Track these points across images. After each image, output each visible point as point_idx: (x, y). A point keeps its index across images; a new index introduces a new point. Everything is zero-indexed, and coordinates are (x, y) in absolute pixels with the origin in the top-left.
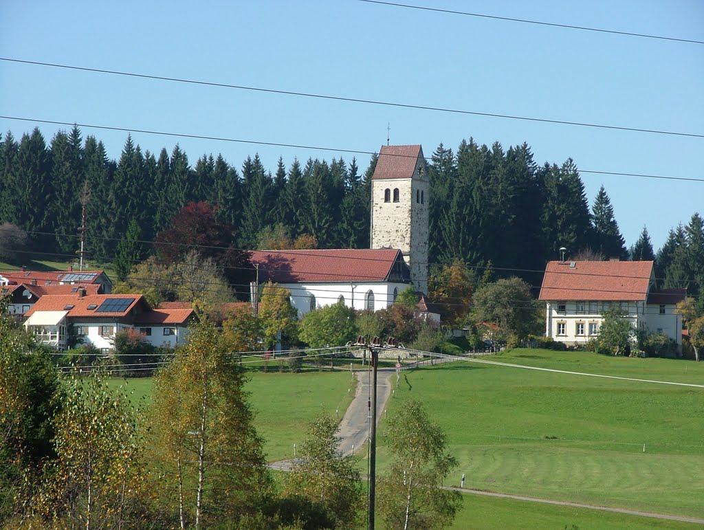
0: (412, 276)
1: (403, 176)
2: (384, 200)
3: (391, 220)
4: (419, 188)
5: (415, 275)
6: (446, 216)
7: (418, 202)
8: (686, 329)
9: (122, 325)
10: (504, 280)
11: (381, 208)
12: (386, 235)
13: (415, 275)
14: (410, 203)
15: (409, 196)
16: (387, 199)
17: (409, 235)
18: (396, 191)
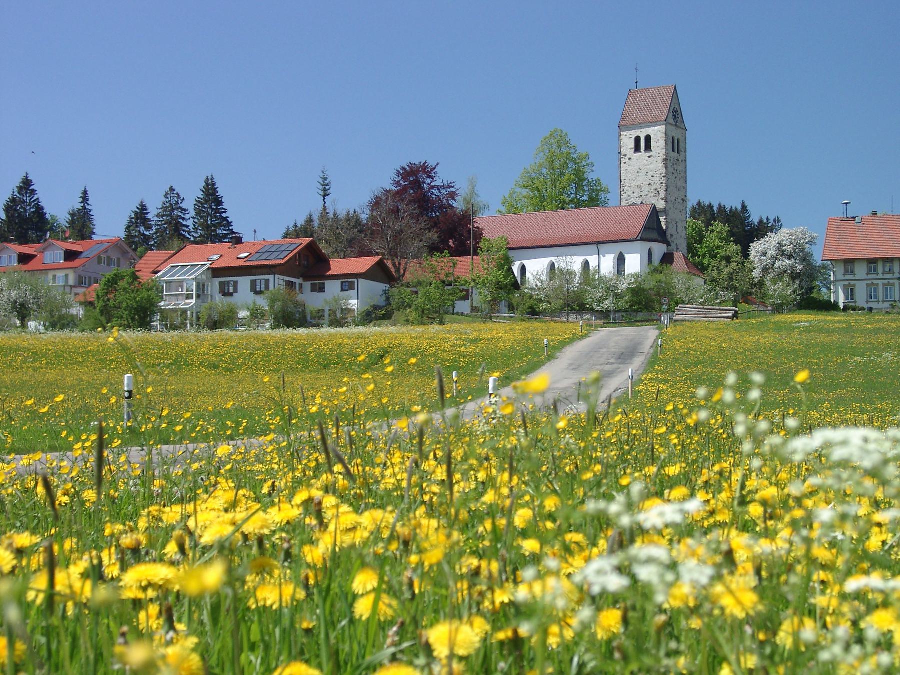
0: (669, 237)
1: (655, 123)
2: (633, 150)
3: (642, 174)
4: (674, 135)
5: (672, 236)
6: (354, 451)
7: (673, 151)
8: (66, 260)
9: (282, 277)
10: (304, 329)
11: (630, 159)
12: (637, 190)
13: (672, 236)
14: (665, 151)
15: (662, 143)
16: (637, 149)
17: (664, 188)
18: (648, 139)
